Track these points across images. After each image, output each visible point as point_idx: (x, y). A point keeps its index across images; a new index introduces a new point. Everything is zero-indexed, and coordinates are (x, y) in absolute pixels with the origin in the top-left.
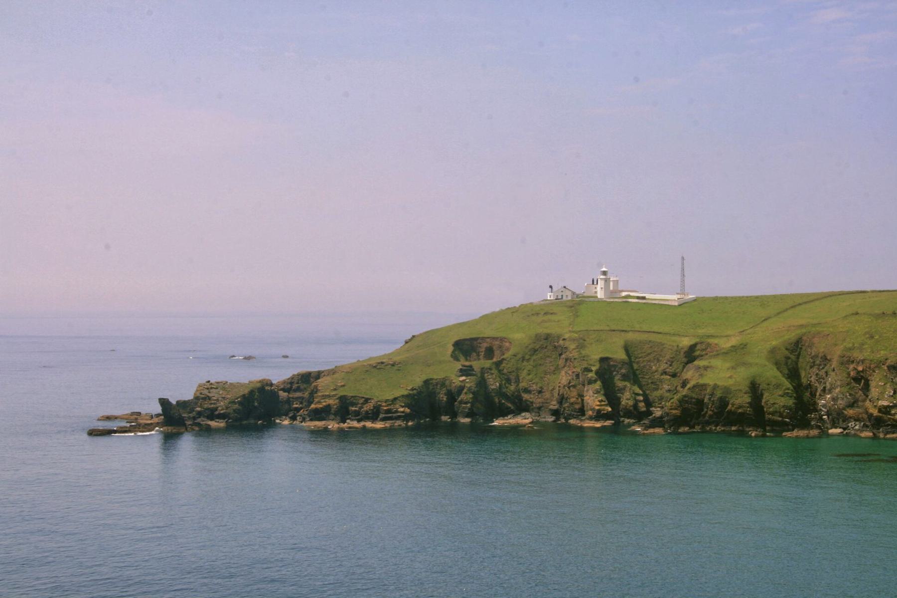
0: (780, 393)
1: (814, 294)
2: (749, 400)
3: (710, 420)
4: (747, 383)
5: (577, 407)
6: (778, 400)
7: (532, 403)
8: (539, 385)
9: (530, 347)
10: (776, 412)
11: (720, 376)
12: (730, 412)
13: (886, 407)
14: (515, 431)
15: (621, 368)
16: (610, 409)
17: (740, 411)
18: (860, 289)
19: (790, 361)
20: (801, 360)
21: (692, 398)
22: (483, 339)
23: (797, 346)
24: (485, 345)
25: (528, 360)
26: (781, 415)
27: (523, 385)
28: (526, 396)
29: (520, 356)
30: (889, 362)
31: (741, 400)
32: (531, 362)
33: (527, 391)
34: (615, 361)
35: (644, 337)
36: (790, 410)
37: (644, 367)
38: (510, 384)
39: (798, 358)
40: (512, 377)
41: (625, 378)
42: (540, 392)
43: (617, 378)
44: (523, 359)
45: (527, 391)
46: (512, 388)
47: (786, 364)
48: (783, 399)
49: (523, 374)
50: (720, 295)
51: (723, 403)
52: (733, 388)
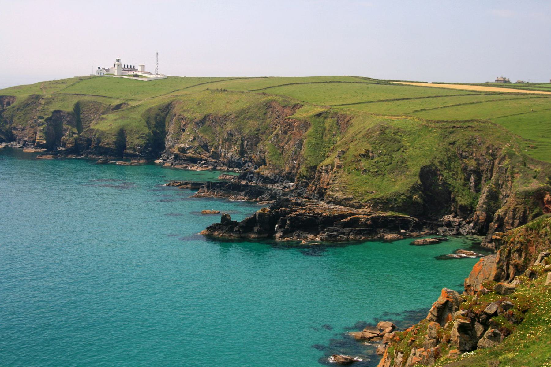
0: (137, 136)
1: (218, 78)
2: (115, 140)
3: (113, 153)
4: (118, 129)
5: (32, 139)
6: (134, 141)
7: (17, 136)
8: (24, 125)
9: (25, 102)
10: (131, 148)
11: (106, 125)
12: (101, 147)
13: (183, 148)
14: (71, 159)
15: (67, 117)
16: (45, 142)
17: (107, 146)
18: (357, 76)
19: (158, 117)
20: (168, 116)
21: (85, 137)
22: (6, 96)
23: (168, 108)
24: (7, 100)
25: (21, 110)
26: (134, 150)
27: (14, 125)
28: (14, 132)
29: (16, 107)
30: (196, 121)
31: (109, 141)
32: (23, 112)
33: (15, 129)
34: (64, 113)
35: (93, 99)
36: (141, 147)
37: (87, 117)
38: (7, 124)
39: (166, 115)
40: (8, 120)
41: (69, 123)
42: (23, 130)
43: (64, 123)
44: (18, 109)
45: (15, 129)
46: (8, 126)
47: (156, 118)
48: (138, 140)
49: (16, 119)
50: (57, 78)
51: (99, 141)
52: (107, 132)
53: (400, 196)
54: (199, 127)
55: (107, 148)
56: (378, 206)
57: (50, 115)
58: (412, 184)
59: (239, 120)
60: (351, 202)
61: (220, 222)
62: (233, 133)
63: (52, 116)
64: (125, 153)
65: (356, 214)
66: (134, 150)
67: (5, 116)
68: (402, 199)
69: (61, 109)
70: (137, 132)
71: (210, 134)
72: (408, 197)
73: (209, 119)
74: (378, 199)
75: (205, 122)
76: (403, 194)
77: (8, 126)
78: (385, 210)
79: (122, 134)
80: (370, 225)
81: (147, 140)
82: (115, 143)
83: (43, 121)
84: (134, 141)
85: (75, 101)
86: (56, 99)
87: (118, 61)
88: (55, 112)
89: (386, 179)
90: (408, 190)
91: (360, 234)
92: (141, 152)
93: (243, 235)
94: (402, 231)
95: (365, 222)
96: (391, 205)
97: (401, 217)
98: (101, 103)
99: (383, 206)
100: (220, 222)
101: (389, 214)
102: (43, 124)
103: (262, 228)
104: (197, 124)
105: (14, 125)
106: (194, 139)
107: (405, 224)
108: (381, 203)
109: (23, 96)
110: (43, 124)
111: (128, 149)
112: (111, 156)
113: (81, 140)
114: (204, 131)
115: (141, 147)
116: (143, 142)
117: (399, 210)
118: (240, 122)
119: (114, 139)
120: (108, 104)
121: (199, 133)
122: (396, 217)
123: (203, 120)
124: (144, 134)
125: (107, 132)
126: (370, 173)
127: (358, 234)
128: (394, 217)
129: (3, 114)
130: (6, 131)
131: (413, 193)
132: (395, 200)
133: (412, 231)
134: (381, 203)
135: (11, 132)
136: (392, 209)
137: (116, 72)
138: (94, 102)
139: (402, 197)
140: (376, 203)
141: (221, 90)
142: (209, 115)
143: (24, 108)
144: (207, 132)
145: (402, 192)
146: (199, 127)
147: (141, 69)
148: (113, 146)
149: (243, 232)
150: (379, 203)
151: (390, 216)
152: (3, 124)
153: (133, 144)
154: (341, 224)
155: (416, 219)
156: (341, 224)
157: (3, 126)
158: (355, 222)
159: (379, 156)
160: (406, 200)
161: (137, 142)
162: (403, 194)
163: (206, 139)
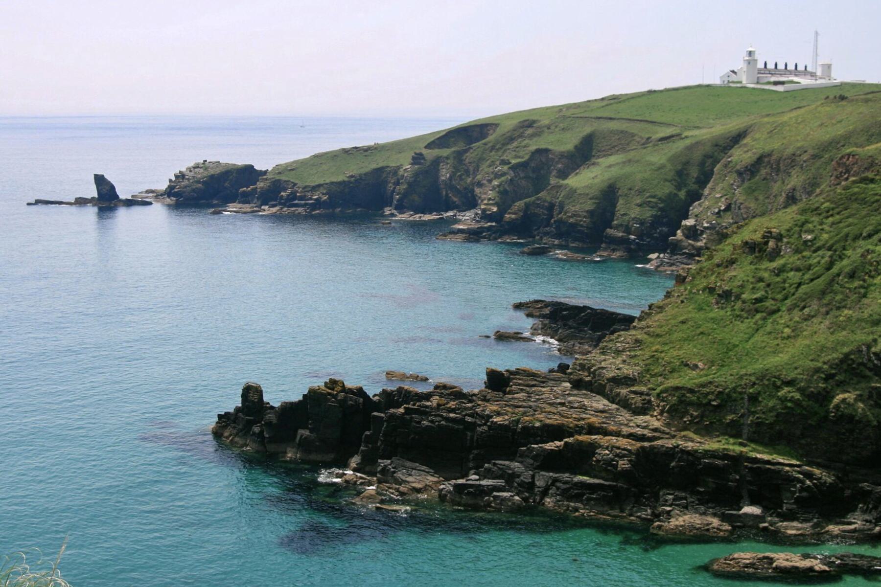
0: (638, 201)
6: (631, 211)
9: (509, 134)
10: (621, 225)
15: (557, 163)
16: (495, 209)
17: (571, 220)
21: (545, 201)
25: (498, 150)
26: (628, 230)
29: (490, 145)
31: (578, 210)
40: (471, 169)
44: (493, 148)
53: (778, 388)
54: (743, 181)
55: (572, 225)
56: (686, 413)
57: (527, 157)
58: (846, 350)
59: (818, 164)
60: (624, 391)
61: (240, 405)
62: (797, 195)
63: (530, 159)
64: (606, 237)
65: (579, 430)
66: (628, 230)
67: (467, 161)
68: (783, 400)
69: (550, 147)
70: (641, 192)
71: (761, 198)
72: (811, 396)
73: (769, 162)
74: (691, 391)
75: (758, 171)
76: (790, 383)
77: (469, 180)
78: (707, 431)
79: (609, 195)
80: (624, 473)
81: (661, 209)
82: (591, 213)
83: (506, 168)
84: (631, 211)
85: (587, 130)
86: (553, 127)
87: (750, 53)
88: (539, 151)
89: (769, 328)
90: (818, 370)
91: (578, 498)
92: (640, 236)
93: (272, 448)
94: (748, 509)
95: (609, 463)
96: (730, 417)
97: (756, 460)
98: (633, 135)
99: (702, 416)
100: (240, 405)
101: (713, 445)
102: (504, 174)
103: (313, 436)
104: (740, 174)
105: (479, 177)
106: (728, 208)
107: (767, 487)
108: (698, 405)
109: (507, 127)
110: (504, 174)
111: (617, 227)
112: (575, 240)
113: (538, 206)
114: (750, 191)
115: (642, 223)
116: (648, 214)
117: (765, 435)
118: (819, 168)
119: (589, 205)
120: (647, 136)
121: (739, 195)
122: (737, 460)
123: (752, 165)
124: (654, 197)
125: (578, 192)
126: (739, 304)
127: (570, 498)
128: (725, 456)
129: (464, 158)
130: (465, 189)
131: (840, 384)
132: (754, 399)
133: (790, 516)
134: (698, 405)
135: (473, 191)
136: (734, 431)
137: (745, 80)
138: (622, 132)
139: (784, 391)
140: (681, 401)
141: (835, 97)
142: (770, 155)
143: (504, 145)
144: (756, 194)
145: (792, 375)
146: (743, 181)
147: (823, 71)
148: (585, 221)
149: (272, 440)
150: (691, 404)
151: (713, 454)
152: (460, 176)
153: (627, 218)
154: (535, 458)
155: (817, 471)
156: (535, 458)
157: (461, 179)
158: (578, 457)
159: (797, 251)
160: (797, 403)
161: (635, 212)
162: (790, 383)
163: (748, 208)
